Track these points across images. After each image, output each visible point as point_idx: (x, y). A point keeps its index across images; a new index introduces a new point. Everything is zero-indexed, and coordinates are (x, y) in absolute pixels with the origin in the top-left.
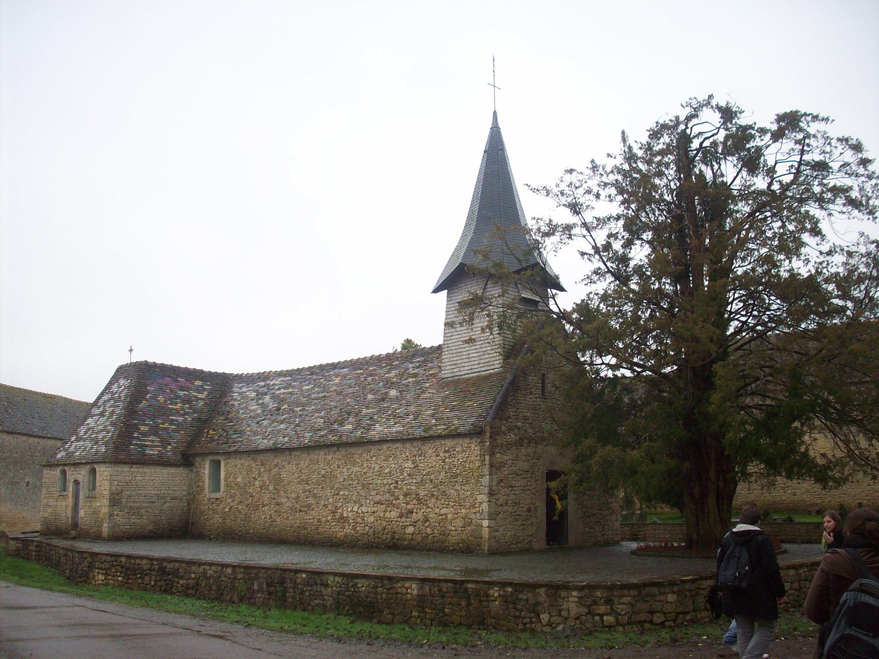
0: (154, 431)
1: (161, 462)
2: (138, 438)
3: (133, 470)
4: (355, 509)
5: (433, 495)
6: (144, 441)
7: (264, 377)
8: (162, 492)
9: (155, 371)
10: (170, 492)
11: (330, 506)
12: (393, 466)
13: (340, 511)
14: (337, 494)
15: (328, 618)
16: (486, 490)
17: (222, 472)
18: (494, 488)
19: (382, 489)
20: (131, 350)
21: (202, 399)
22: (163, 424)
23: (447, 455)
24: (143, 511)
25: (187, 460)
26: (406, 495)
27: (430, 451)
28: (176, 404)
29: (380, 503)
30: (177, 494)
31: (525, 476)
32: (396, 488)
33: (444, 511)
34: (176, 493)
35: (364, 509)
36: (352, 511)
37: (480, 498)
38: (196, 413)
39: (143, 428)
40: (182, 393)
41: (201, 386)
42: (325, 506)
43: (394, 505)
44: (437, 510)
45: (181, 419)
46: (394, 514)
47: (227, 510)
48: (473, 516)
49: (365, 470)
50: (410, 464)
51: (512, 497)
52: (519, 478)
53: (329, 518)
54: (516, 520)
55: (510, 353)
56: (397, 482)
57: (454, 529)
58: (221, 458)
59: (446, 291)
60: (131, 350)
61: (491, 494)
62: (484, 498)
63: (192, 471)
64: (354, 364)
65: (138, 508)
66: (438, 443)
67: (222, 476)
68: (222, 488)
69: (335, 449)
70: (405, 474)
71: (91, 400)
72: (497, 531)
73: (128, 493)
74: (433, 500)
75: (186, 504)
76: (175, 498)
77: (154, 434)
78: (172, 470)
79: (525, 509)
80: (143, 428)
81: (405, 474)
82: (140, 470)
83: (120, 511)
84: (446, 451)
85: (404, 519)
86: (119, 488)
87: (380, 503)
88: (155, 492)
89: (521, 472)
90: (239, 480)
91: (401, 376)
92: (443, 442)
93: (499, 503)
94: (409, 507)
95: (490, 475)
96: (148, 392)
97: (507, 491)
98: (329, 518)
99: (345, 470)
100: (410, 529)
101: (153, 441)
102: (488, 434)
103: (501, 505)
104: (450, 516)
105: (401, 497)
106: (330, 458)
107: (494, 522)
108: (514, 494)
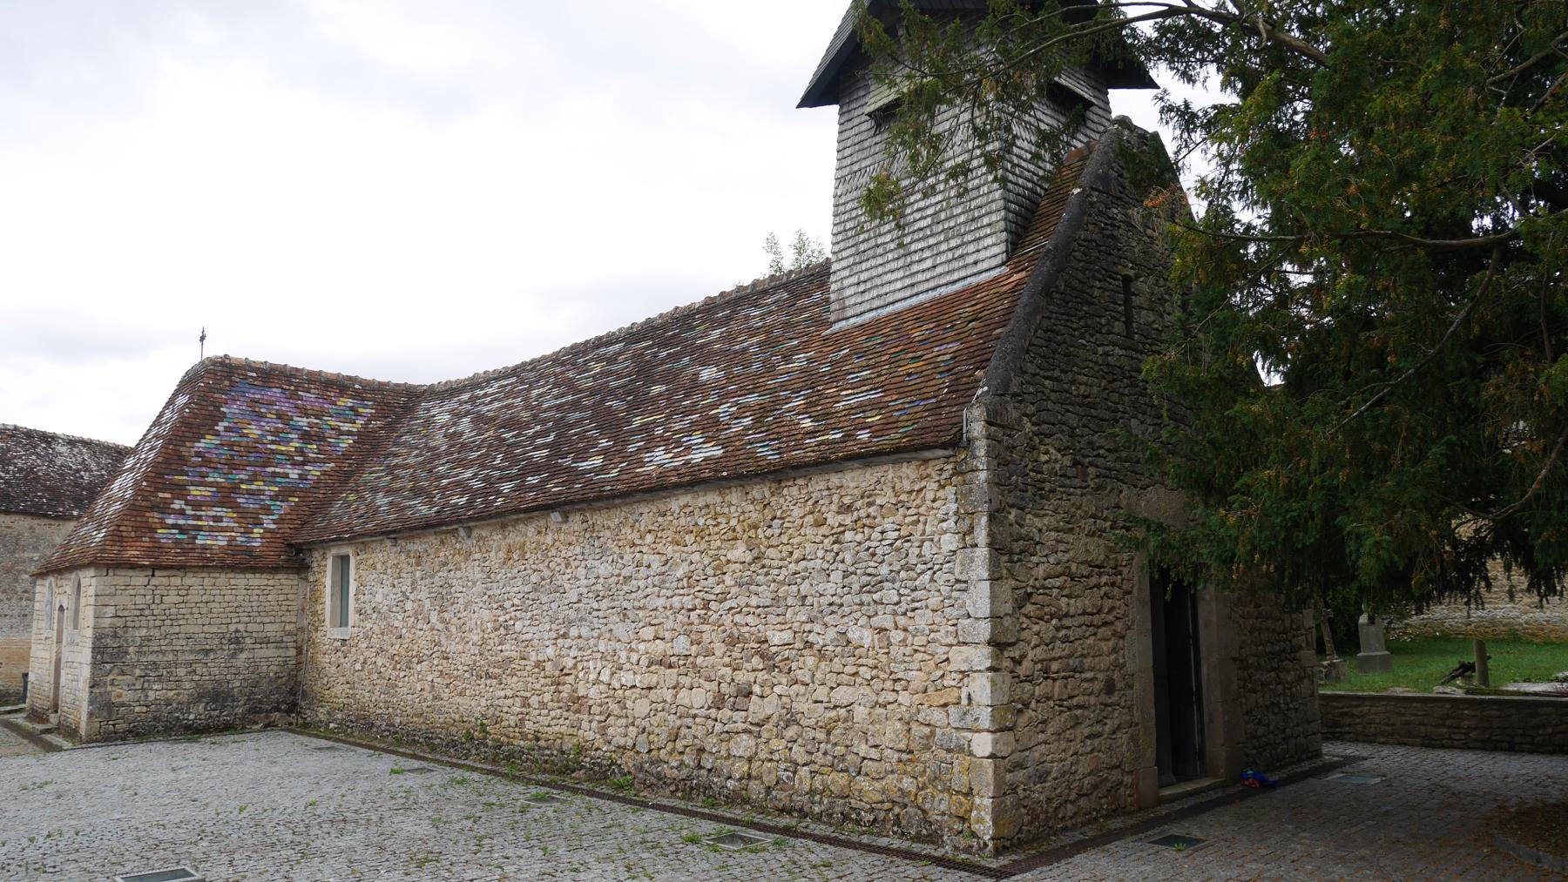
0: (226, 496)
1: (240, 562)
2: (182, 513)
3: (154, 581)
4: (605, 678)
5: (809, 645)
6: (199, 518)
7: (474, 383)
8: (232, 628)
9: (246, 377)
10: (251, 627)
11: (548, 666)
12: (696, 557)
13: (570, 679)
14: (564, 636)
15: (868, 496)
16: (984, 630)
17: (352, 581)
18: (1007, 622)
19: (669, 624)
20: (202, 338)
21: (349, 433)
22: (250, 481)
23: (848, 519)
24: (181, 672)
25: (294, 557)
26: (732, 641)
27: (797, 512)
28: (288, 442)
29: (664, 662)
30: (272, 630)
31: (1093, 581)
32: (704, 620)
33: (843, 695)
34: (268, 627)
35: (627, 678)
36: (597, 682)
37: (959, 658)
38: (330, 460)
39: (196, 492)
40: (303, 422)
41: (351, 408)
42: (538, 664)
43: (698, 670)
44: (822, 693)
45: (294, 474)
46: (698, 698)
47: (358, 666)
48: (937, 716)
49: (625, 572)
50: (739, 552)
51: (1060, 649)
52: (1078, 589)
53: (547, 697)
54: (1077, 723)
55: (1023, 225)
56: (706, 607)
57: (874, 754)
58: (349, 551)
59: (836, 108)
60: (202, 338)
61: (998, 644)
62: (981, 657)
63: (306, 579)
64: (633, 335)
65: (169, 664)
66: (818, 485)
67: (352, 591)
68: (353, 617)
69: (556, 517)
70: (729, 581)
71: (133, 446)
72: (1019, 766)
73: (143, 632)
74: (811, 661)
75: (293, 652)
76: (265, 641)
77: (222, 504)
78: (257, 580)
79: (1097, 686)
80: (196, 492)
81: (729, 581)
82: (176, 581)
83: (123, 673)
84: (846, 509)
85: (726, 713)
86: (119, 623)
87: (664, 662)
88: (214, 629)
89: (1085, 570)
90: (379, 598)
91: (729, 338)
92: (835, 480)
93: (1025, 668)
94: (742, 677)
95: (994, 579)
96: (223, 417)
97: (1047, 629)
98: (547, 697)
99: (581, 572)
100: (743, 745)
101: (218, 519)
102: (981, 448)
103: (1029, 679)
104: (860, 712)
105: (719, 648)
106: (549, 540)
107: (1009, 736)
108: (1066, 640)
